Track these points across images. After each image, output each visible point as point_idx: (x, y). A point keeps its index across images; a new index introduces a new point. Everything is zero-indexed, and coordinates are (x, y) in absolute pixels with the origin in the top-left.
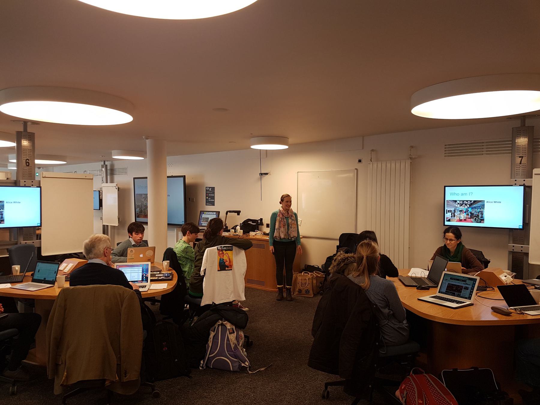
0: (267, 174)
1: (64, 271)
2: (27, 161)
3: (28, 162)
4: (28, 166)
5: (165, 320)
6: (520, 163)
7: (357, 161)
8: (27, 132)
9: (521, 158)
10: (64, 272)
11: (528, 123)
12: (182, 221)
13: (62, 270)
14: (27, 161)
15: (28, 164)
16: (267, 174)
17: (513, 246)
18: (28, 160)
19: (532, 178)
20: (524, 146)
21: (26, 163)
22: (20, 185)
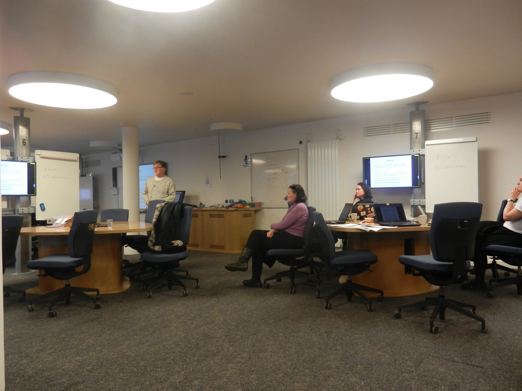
0: (276, 178)
1: (61, 223)
2: (24, 141)
3: (24, 142)
4: (25, 145)
5: (464, 308)
6: (416, 138)
7: (298, 142)
8: (412, 274)
9: (416, 134)
10: (61, 224)
11: (421, 108)
12: (78, 158)
13: (58, 224)
14: (24, 141)
15: (24, 144)
16: (276, 178)
17: (414, 201)
18: (25, 140)
19: (424, 148)
20: (415, 118)
21: (23, 142)
22: (18, 159)
